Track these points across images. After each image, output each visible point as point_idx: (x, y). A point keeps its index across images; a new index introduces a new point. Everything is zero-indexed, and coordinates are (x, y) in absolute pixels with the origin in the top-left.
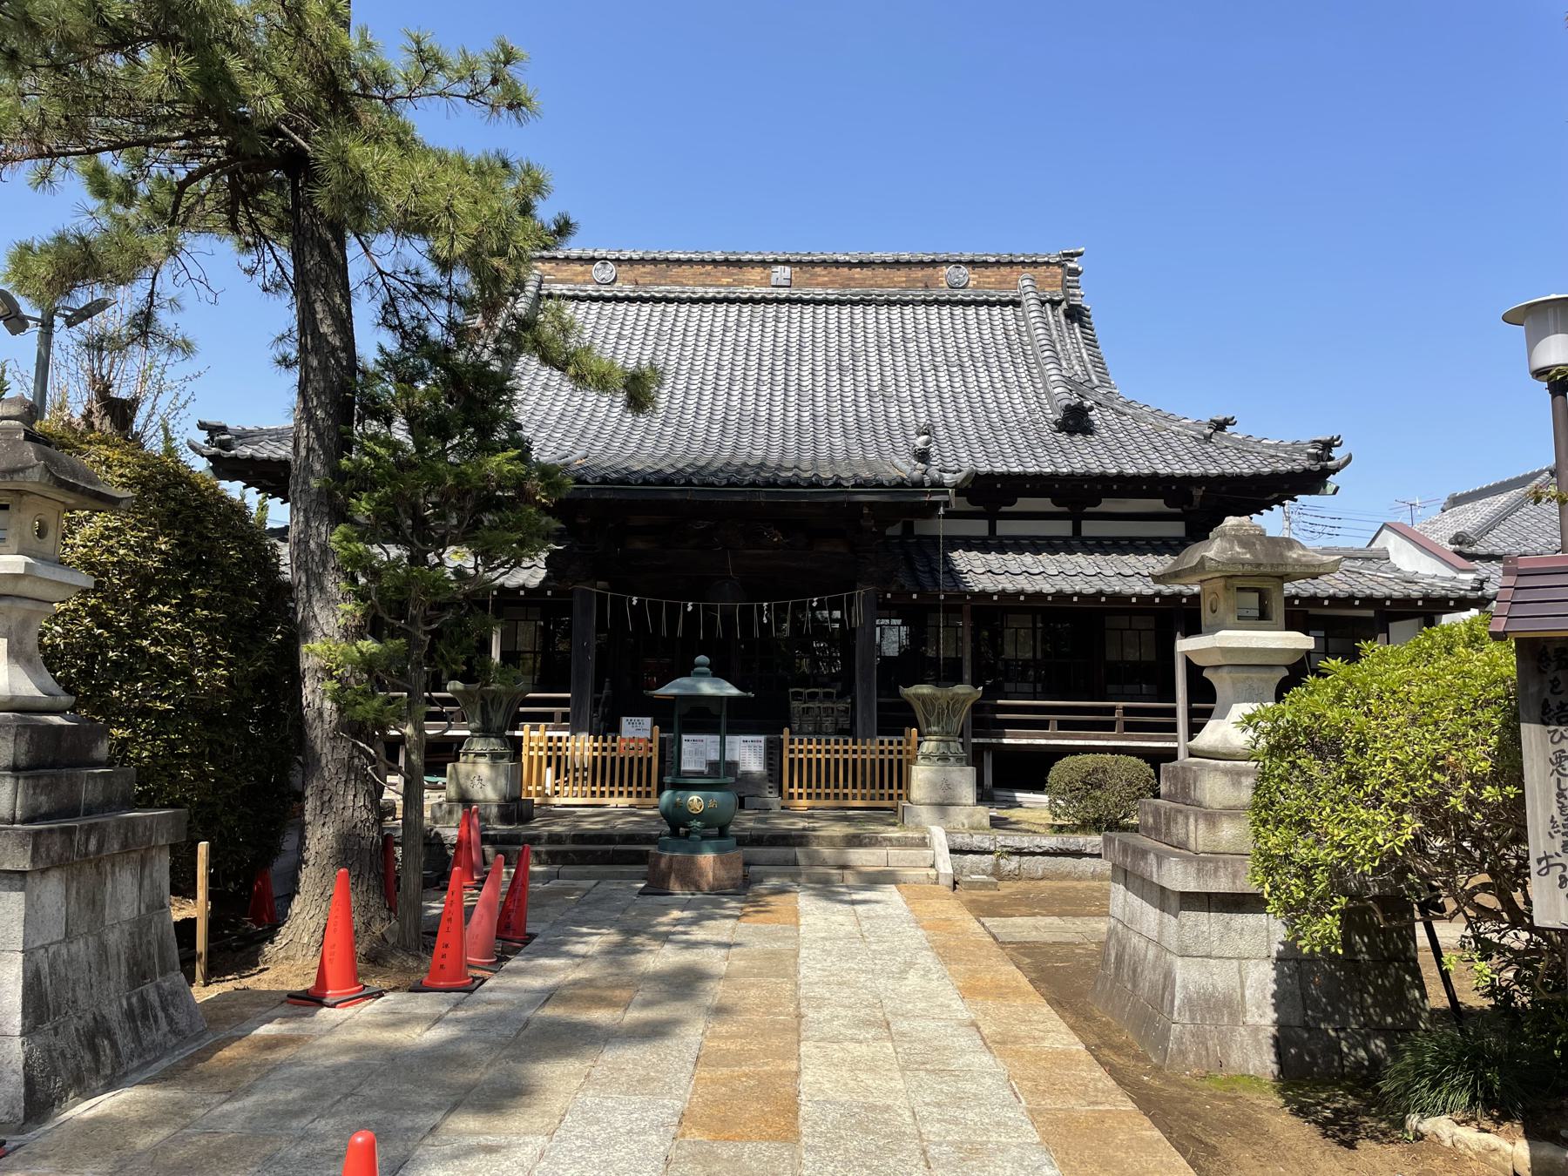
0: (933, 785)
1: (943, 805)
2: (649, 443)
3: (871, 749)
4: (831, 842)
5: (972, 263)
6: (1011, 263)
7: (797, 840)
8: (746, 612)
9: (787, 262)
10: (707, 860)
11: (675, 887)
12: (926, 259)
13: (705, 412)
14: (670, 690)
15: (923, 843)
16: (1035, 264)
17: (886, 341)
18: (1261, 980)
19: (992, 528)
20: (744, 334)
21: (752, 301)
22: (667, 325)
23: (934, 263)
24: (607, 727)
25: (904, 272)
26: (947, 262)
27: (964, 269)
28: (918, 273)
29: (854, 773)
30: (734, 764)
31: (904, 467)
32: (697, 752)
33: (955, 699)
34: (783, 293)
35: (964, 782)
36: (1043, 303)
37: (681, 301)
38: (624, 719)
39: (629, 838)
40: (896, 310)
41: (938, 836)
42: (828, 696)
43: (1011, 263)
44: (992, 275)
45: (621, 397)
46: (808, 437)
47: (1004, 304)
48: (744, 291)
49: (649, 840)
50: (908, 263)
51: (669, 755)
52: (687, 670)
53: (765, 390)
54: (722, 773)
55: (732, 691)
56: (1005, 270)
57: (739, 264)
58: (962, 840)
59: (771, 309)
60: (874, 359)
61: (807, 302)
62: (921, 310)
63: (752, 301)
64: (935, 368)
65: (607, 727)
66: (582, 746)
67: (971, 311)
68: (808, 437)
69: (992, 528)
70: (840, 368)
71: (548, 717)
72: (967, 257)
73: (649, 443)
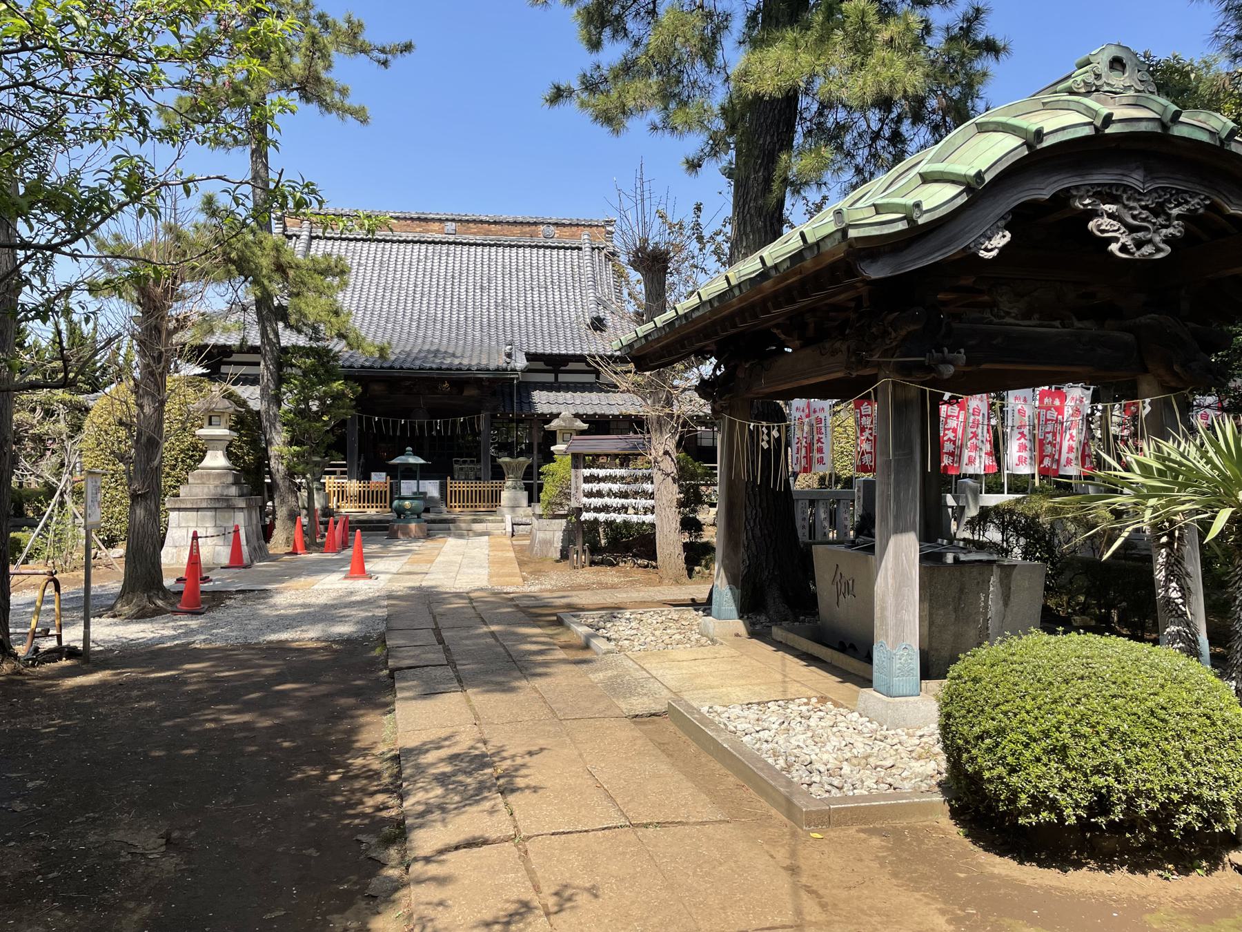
0: (510, 499)
1: (514, 508)
2: (380, 334)
3: (487, 486)
4: (465, 521)
5: (556, 224)
6: (577, 225)
7: (453, 521)
8: (430, 424)
9: (453, 220)
10: (413, 526)
11: (400, 535)
12: (531, 221)
13: (408, 314)
14: (396, 461)
15: (502, 521)
16: (590, 226)
17: (507, 270)
18: (559, 535)
19: (556, 378)
20: (429, 264)
21: (433, 242)
22: (386, 257)
23: (535, 224)
24: (365, 477)
25: (519, 227)
26: (543, 223)
27: (552, 228)
28: (527, 229)
29: (480, 496)
30: (425, 493)
31: (501, 361)
32: (408, 487)
33: (519, 463)
34: (452, 238)
35: (523, 496)
36: (593, 249)
37: (393, 242)
38: (373, 474)
39: (380, 521)
40: (514, 250)
41: (508, 518)
42: (472, 462)
43: (577, 225)
44: (567, 231)
45: (303, 144)
46: (462, 332)
47: (573, 249)
48: (429, 237)
49: (388, 522)
50: (521, 223)
51: (394, 491)
52: (403, 453)
53: (440, 300)
54: (420, 495)
55: (422, 461)
56: (574, 229)
57: (426, 220)
58: (517, 520)
59: (445, 247)
60: (500, 282)
61: (465, 244)
62: (528, 250)
63: (433, 242)
64: (532, 289)
65: (365, 477)
66: (353, 486)
67: (555, 252)
68: (462, 332)
69: (556, 378)
70: (482, 288)
71: (334, 473)
72: (553, 221)
73: (380, 334)
